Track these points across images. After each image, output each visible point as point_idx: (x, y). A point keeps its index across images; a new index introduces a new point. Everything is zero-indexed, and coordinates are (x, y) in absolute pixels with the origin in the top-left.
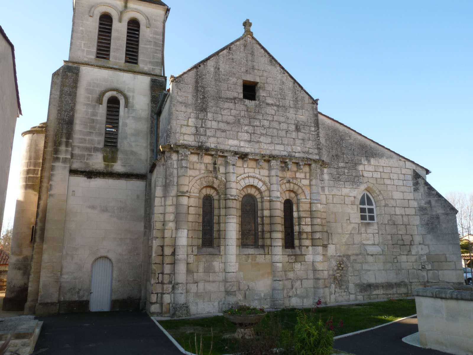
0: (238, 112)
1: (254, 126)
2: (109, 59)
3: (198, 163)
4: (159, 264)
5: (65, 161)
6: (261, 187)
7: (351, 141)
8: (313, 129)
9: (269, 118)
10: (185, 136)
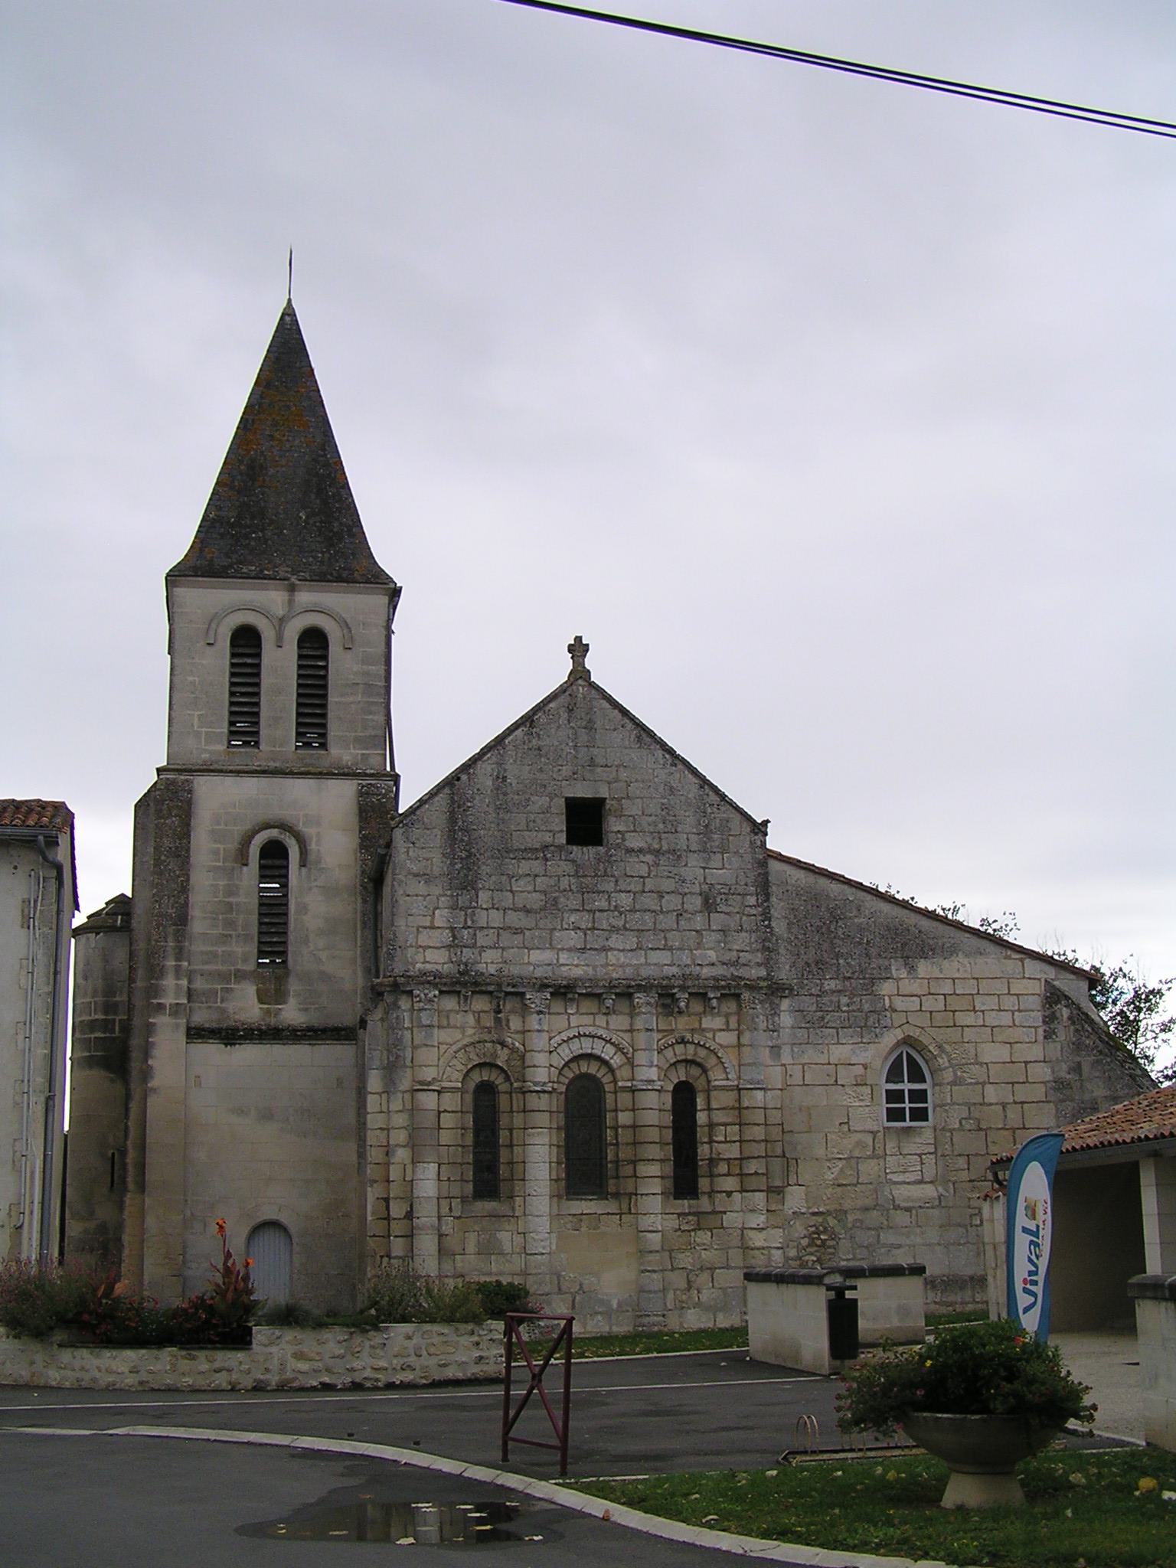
0: (552, 882)
1: (592, 912)
2: (257, 744)
3: (457, 1012)
4: (383, 1237)
5: (176, 1010)
6: (611, 1058)
7: (862, 920)
8: (752, 900)
9: (632, 887)
10: (428, 952)
